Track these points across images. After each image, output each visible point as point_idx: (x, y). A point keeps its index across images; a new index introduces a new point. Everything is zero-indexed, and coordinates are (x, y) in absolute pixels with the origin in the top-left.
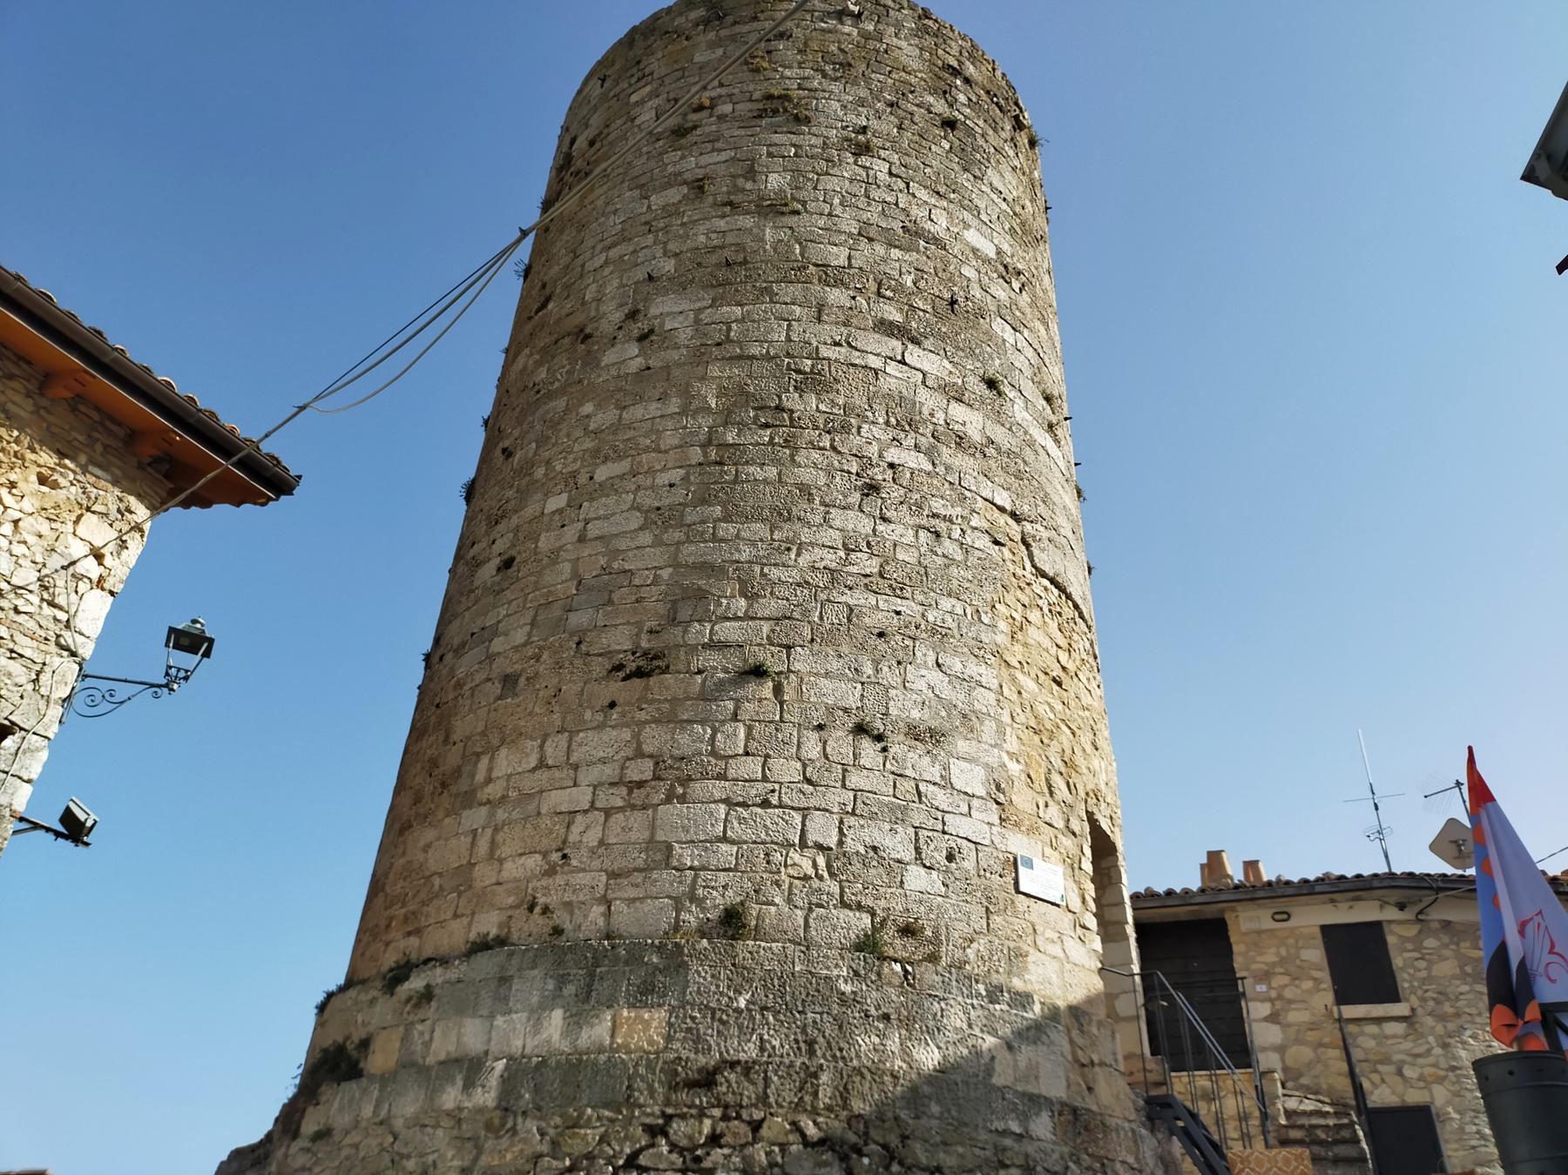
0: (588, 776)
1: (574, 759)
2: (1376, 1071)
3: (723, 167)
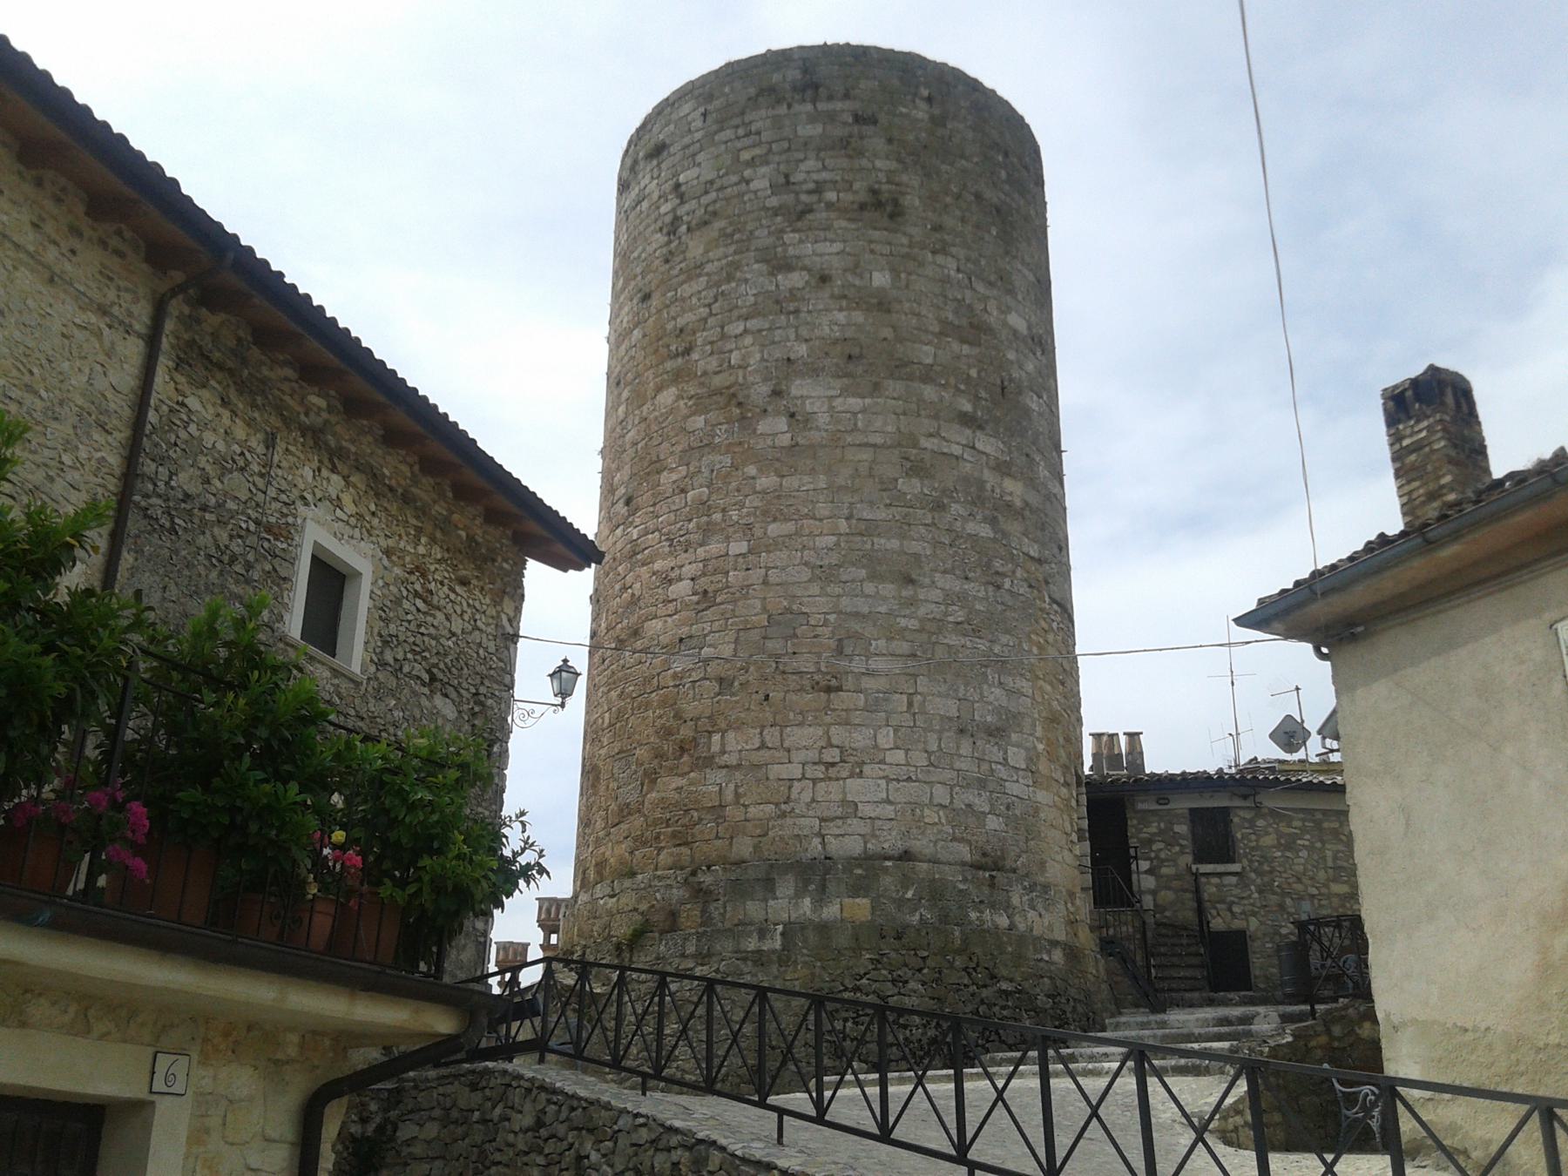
0: (798, 756)
2: (1216, 908)
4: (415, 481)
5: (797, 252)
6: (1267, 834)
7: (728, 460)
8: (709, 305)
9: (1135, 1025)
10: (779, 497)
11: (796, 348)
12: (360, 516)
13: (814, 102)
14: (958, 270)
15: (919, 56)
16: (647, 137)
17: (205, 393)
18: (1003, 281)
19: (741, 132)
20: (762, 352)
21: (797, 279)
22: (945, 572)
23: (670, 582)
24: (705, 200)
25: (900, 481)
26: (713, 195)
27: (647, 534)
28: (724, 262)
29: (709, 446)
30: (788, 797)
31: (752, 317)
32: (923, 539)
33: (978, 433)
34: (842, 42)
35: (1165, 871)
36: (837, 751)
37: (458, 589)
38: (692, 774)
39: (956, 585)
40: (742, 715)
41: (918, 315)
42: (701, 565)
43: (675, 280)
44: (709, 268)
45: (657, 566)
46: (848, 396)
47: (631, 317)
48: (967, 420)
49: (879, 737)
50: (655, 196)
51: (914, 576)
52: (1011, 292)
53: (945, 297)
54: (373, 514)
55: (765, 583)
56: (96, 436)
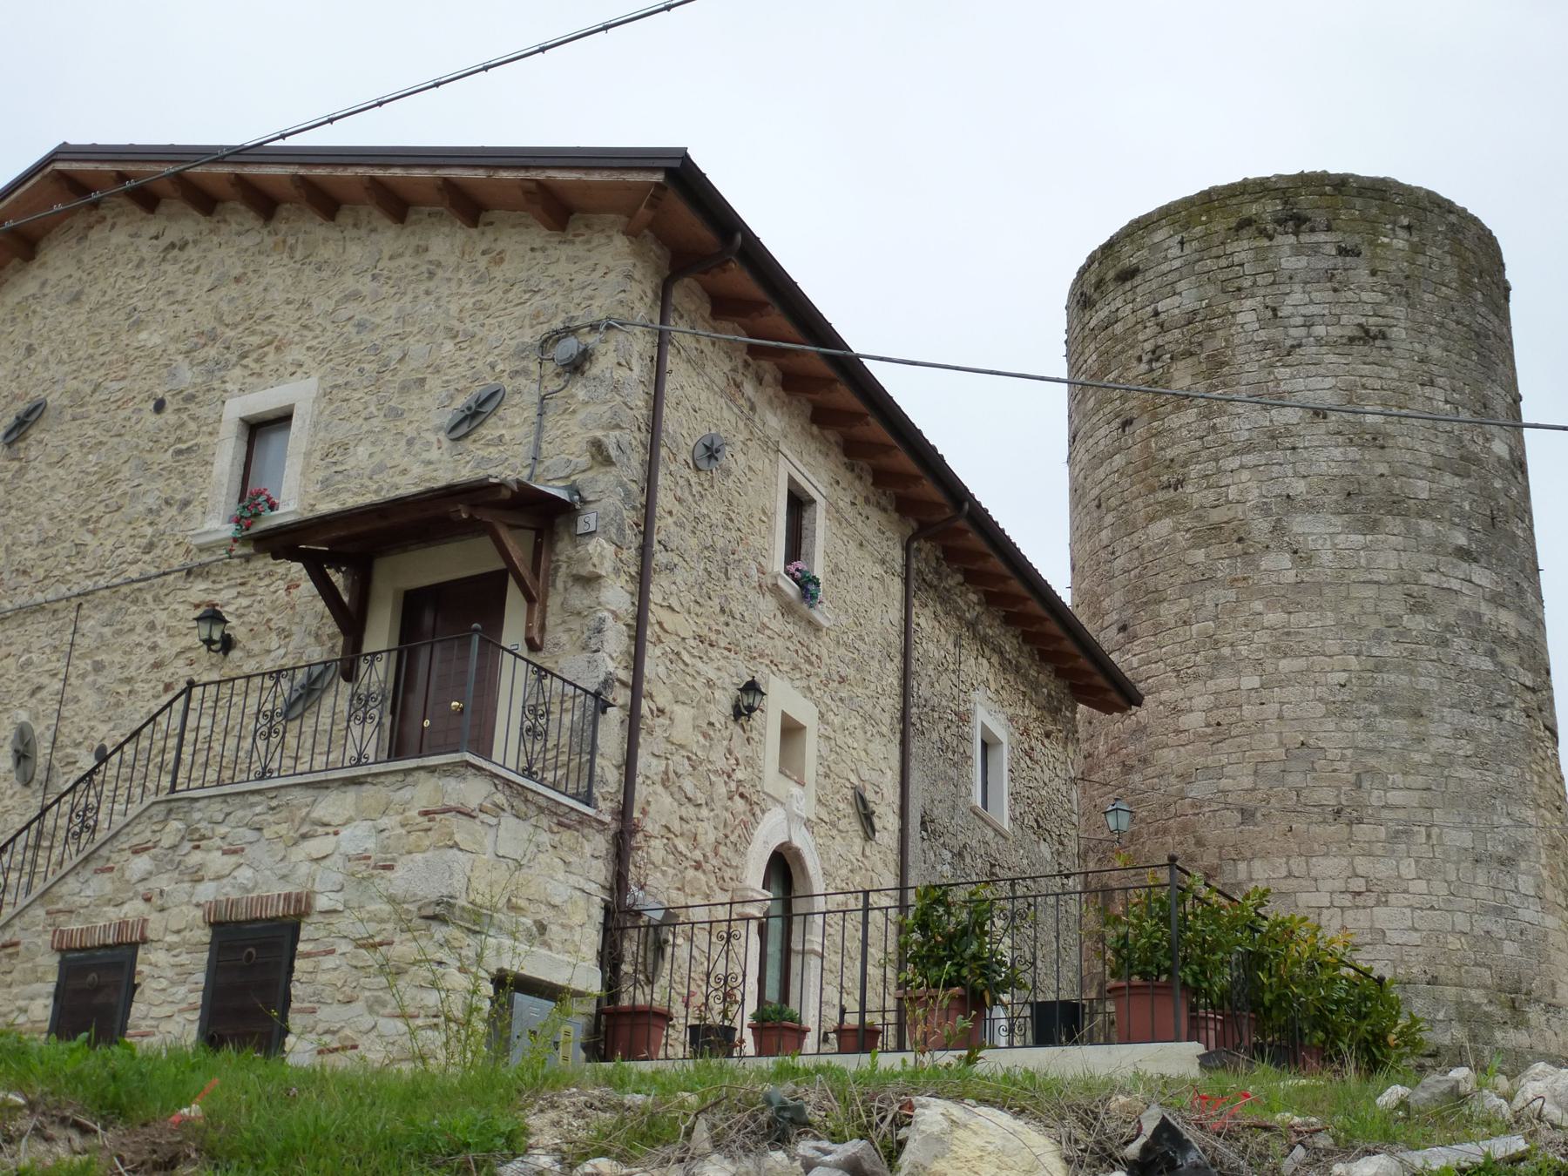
1: (1313, 873)
3: (1329, 392)
11: (1294, 485)
21: (1291, 416)
22: (1452, 707)
27: (1150, 663)
29: (1209, 579)
31: (1248, 452)
32: (1429, 675)
33: (1474, 565)
36: (1363, 881)
39: (1467, 720)
46: (1349, 533)
48: (1464, 554)
55: (1280, 717)
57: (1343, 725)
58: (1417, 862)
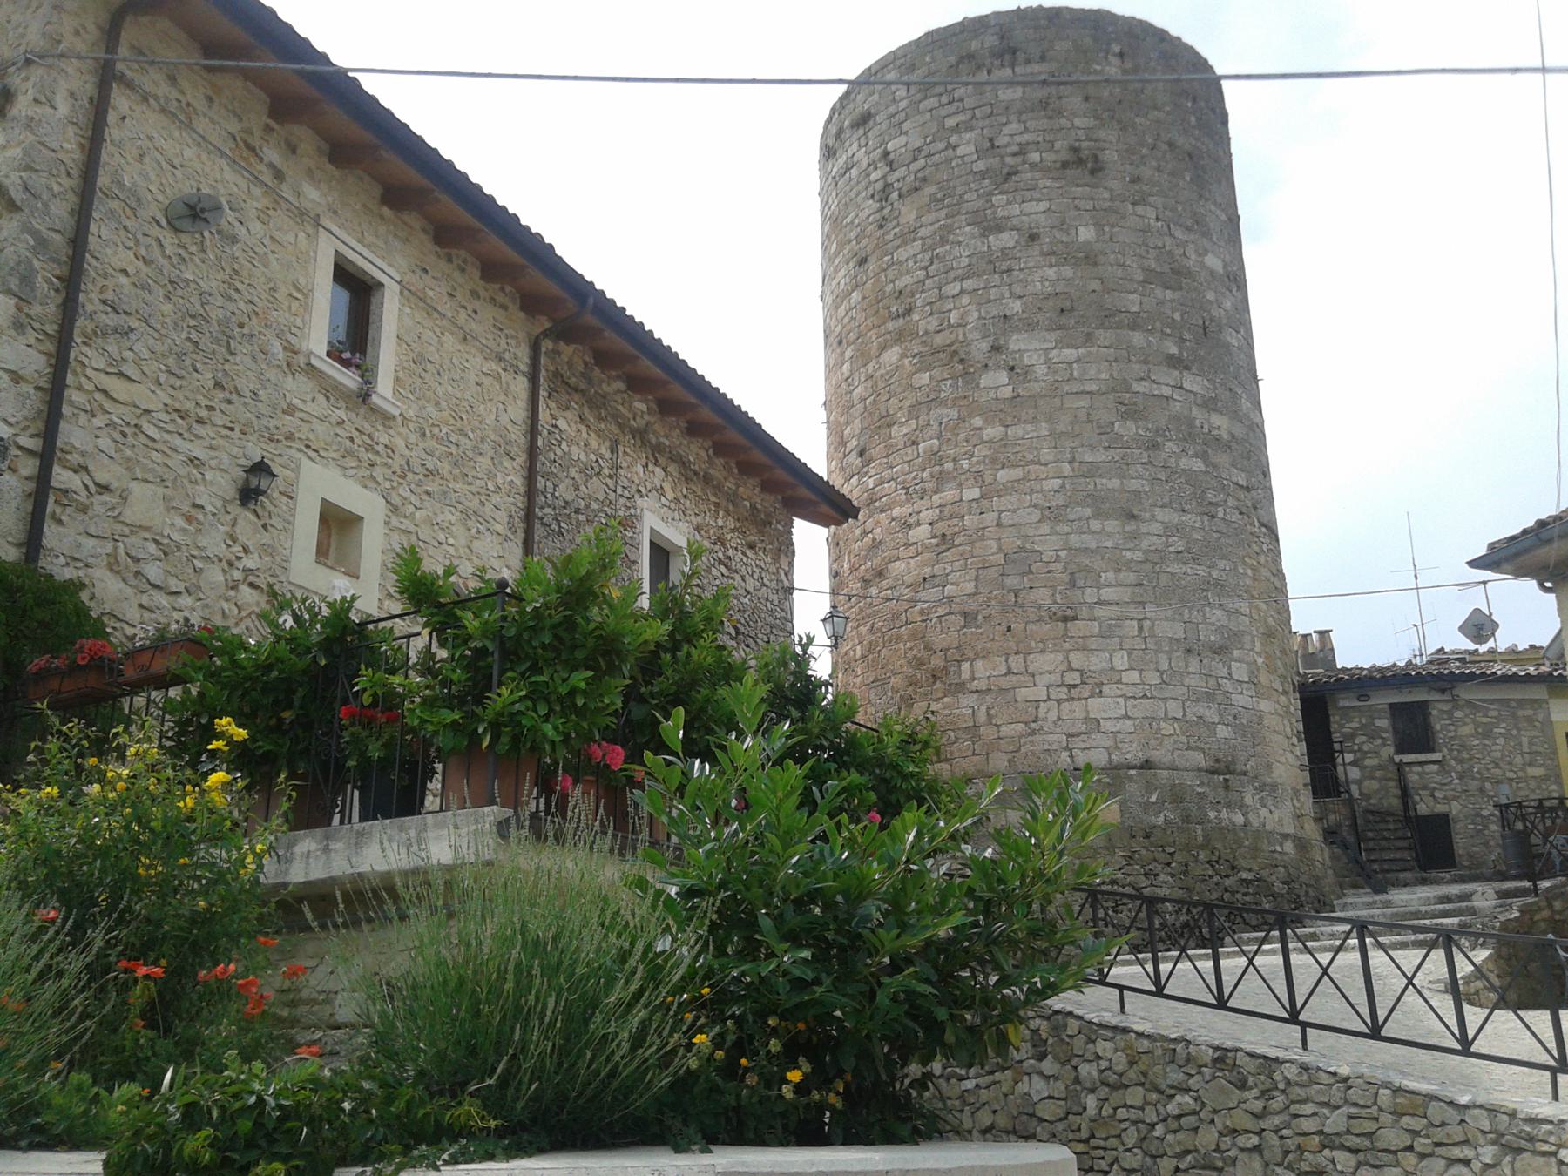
0: (1043, 680)
3: (1043, 216)
4: (711, 463)
5: (1006, 214)
6: (1465, 724)
7: (954, 413)
8: (926, 268)
9: (1359, 904)
10: (1005, 446)
12: (677, 500)
13: (1013, 66)
14: (1158, 219)
15: (1108, 13)
16: (851, 106)
17: (569, 414)
18: (1199, 225)
19: (944, 99)
20: (979, 311)
21: (1007, 239)
23: (910, 527)
24: (914, 167)
25: (1117, 424)
26: (922, 162)
27: (883, 483)
28: (937, 226)
29: (933, 401)
30: (1037, 717)
31: (968, 278)
32: (1140, 477)
34: (1035, 5)
35: (1368, 762)
36: (1078, 674)
37: (748, 552)
38: (946, 700)
39: (1175, 518)
40: (988, 645)
41: (1123, 265)
42: (937, 511)
43: (890, 245)
44: (922, 232)
45: (896, 512)
46: (1063, 348)
47: (848, 280)
48: (1174, 362)
49: (1115, 660)
50: (865, 163)
51: (1135, 512)
52: (1206, 234)
53: (1147, 246)
54: (685, 497)
55: (999, 525)
56: (505, 464)
57: (1058, 528)
58: (1130, 654)
